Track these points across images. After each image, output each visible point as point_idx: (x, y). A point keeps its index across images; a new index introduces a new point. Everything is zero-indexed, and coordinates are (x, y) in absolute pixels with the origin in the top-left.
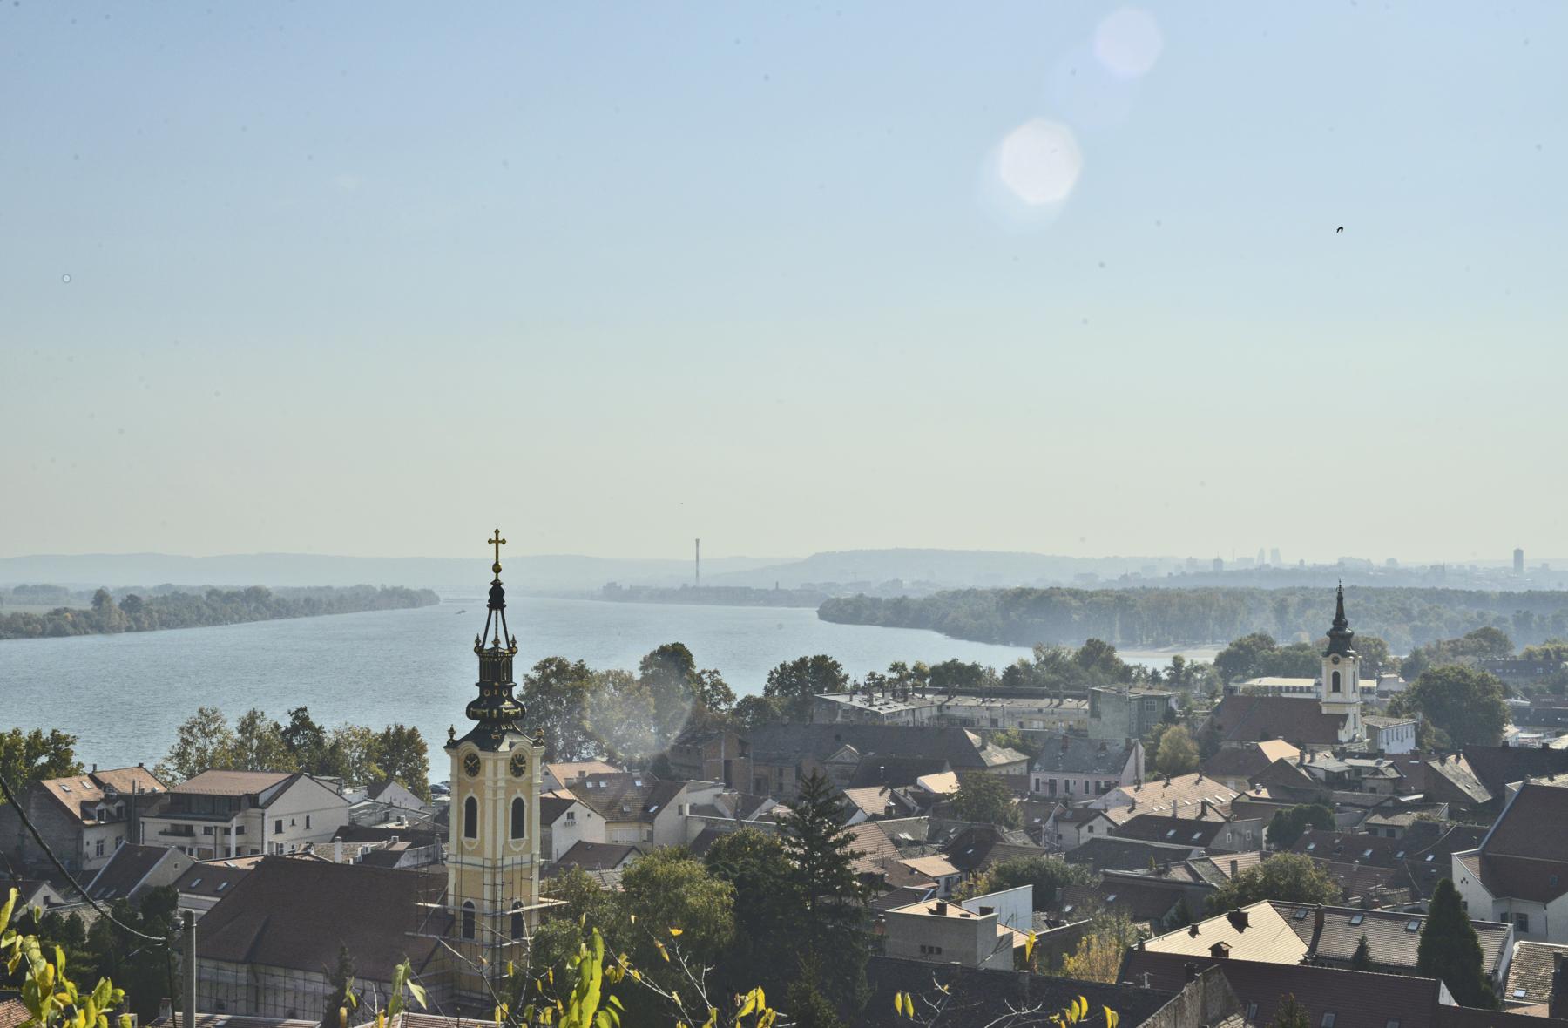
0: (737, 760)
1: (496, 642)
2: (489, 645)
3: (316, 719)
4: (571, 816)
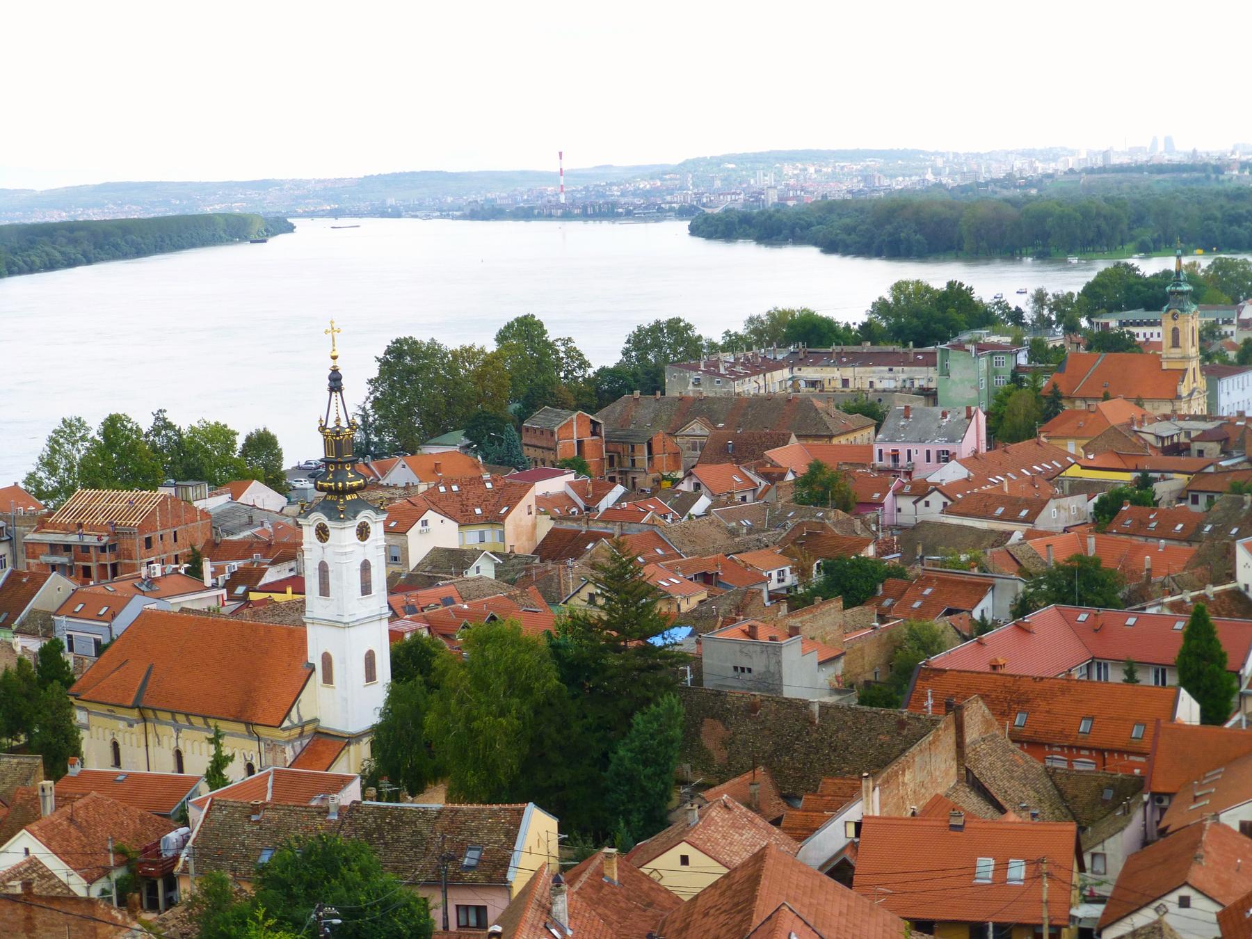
0: (588, 439)
1: (338, 420)
2: (331, 424)
3: (171, 417)
4: (425, 523)
